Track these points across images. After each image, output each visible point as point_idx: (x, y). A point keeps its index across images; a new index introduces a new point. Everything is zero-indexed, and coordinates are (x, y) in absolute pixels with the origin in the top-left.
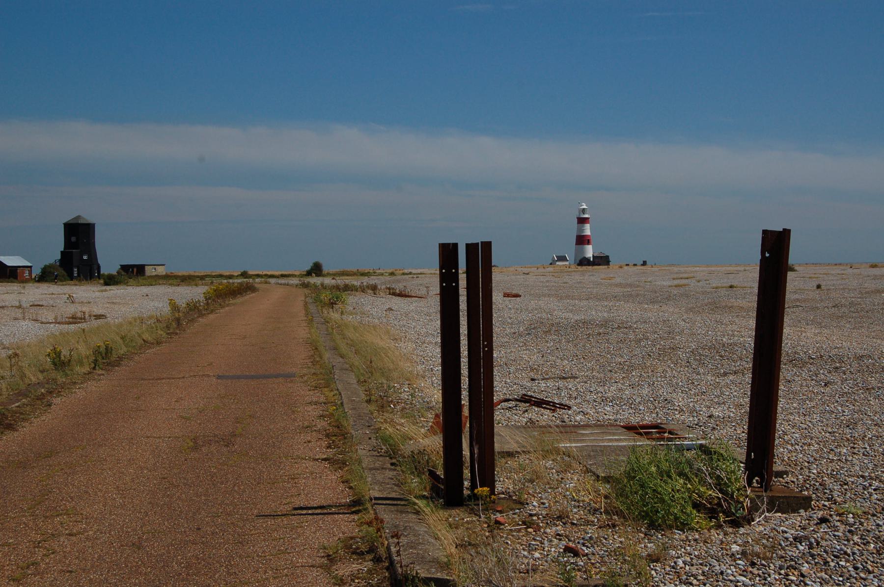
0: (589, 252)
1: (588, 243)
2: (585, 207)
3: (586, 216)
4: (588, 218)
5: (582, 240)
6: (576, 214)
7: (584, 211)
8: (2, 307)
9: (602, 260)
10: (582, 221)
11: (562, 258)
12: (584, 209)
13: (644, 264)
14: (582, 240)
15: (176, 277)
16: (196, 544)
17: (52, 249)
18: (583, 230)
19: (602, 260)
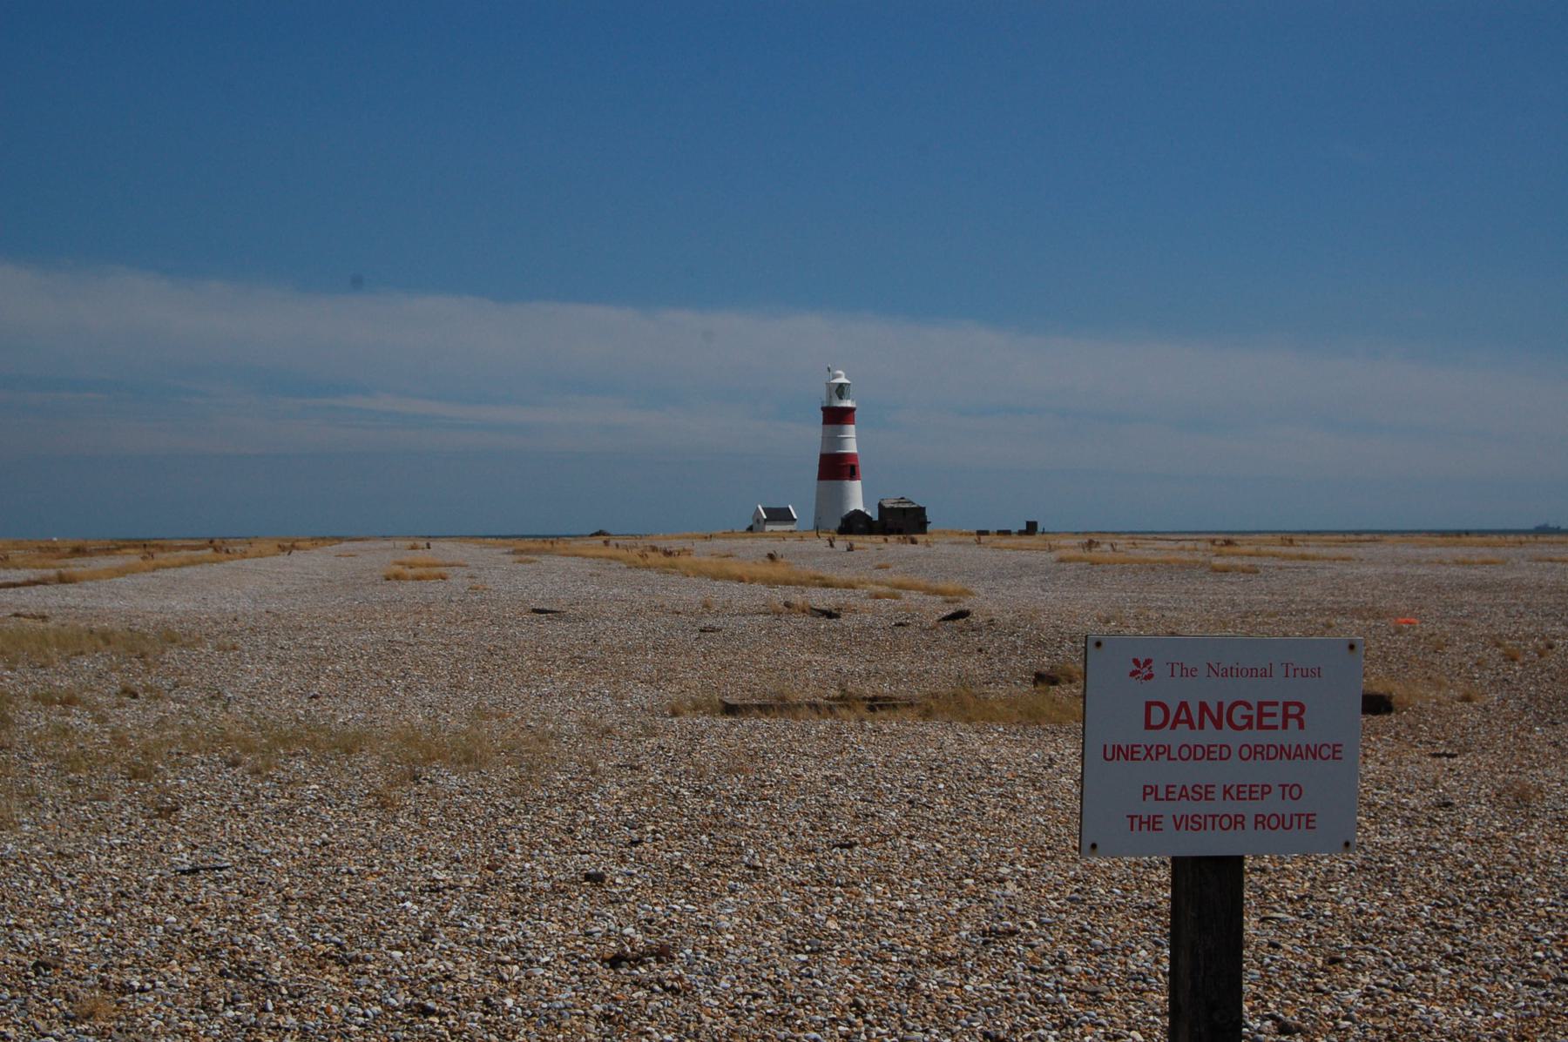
0: (857, 497)
1: (853, 473)
2: (843, 380)
3: (848, 404)
4: (851, 410)
5: (837, 467)
6: (821, 397)
7: (841, 390)
8: (1564, 561)
9: (903, 521)
10: (836, 417)
11: (779, 515)
12: (841, 385)
13: (1031, 528)
14: (837, 467)
15: (324, 538)
16: (851, 846)
17: (1024, 527)
18: (840, 442)
19: (903, 521)
